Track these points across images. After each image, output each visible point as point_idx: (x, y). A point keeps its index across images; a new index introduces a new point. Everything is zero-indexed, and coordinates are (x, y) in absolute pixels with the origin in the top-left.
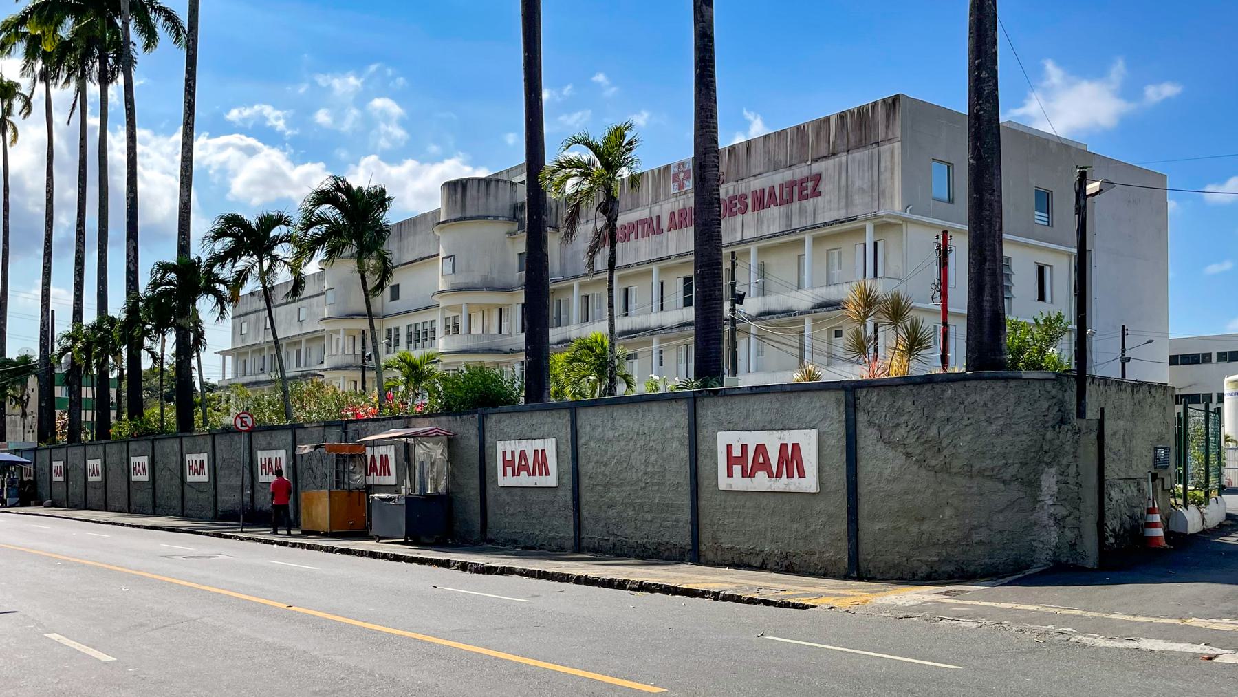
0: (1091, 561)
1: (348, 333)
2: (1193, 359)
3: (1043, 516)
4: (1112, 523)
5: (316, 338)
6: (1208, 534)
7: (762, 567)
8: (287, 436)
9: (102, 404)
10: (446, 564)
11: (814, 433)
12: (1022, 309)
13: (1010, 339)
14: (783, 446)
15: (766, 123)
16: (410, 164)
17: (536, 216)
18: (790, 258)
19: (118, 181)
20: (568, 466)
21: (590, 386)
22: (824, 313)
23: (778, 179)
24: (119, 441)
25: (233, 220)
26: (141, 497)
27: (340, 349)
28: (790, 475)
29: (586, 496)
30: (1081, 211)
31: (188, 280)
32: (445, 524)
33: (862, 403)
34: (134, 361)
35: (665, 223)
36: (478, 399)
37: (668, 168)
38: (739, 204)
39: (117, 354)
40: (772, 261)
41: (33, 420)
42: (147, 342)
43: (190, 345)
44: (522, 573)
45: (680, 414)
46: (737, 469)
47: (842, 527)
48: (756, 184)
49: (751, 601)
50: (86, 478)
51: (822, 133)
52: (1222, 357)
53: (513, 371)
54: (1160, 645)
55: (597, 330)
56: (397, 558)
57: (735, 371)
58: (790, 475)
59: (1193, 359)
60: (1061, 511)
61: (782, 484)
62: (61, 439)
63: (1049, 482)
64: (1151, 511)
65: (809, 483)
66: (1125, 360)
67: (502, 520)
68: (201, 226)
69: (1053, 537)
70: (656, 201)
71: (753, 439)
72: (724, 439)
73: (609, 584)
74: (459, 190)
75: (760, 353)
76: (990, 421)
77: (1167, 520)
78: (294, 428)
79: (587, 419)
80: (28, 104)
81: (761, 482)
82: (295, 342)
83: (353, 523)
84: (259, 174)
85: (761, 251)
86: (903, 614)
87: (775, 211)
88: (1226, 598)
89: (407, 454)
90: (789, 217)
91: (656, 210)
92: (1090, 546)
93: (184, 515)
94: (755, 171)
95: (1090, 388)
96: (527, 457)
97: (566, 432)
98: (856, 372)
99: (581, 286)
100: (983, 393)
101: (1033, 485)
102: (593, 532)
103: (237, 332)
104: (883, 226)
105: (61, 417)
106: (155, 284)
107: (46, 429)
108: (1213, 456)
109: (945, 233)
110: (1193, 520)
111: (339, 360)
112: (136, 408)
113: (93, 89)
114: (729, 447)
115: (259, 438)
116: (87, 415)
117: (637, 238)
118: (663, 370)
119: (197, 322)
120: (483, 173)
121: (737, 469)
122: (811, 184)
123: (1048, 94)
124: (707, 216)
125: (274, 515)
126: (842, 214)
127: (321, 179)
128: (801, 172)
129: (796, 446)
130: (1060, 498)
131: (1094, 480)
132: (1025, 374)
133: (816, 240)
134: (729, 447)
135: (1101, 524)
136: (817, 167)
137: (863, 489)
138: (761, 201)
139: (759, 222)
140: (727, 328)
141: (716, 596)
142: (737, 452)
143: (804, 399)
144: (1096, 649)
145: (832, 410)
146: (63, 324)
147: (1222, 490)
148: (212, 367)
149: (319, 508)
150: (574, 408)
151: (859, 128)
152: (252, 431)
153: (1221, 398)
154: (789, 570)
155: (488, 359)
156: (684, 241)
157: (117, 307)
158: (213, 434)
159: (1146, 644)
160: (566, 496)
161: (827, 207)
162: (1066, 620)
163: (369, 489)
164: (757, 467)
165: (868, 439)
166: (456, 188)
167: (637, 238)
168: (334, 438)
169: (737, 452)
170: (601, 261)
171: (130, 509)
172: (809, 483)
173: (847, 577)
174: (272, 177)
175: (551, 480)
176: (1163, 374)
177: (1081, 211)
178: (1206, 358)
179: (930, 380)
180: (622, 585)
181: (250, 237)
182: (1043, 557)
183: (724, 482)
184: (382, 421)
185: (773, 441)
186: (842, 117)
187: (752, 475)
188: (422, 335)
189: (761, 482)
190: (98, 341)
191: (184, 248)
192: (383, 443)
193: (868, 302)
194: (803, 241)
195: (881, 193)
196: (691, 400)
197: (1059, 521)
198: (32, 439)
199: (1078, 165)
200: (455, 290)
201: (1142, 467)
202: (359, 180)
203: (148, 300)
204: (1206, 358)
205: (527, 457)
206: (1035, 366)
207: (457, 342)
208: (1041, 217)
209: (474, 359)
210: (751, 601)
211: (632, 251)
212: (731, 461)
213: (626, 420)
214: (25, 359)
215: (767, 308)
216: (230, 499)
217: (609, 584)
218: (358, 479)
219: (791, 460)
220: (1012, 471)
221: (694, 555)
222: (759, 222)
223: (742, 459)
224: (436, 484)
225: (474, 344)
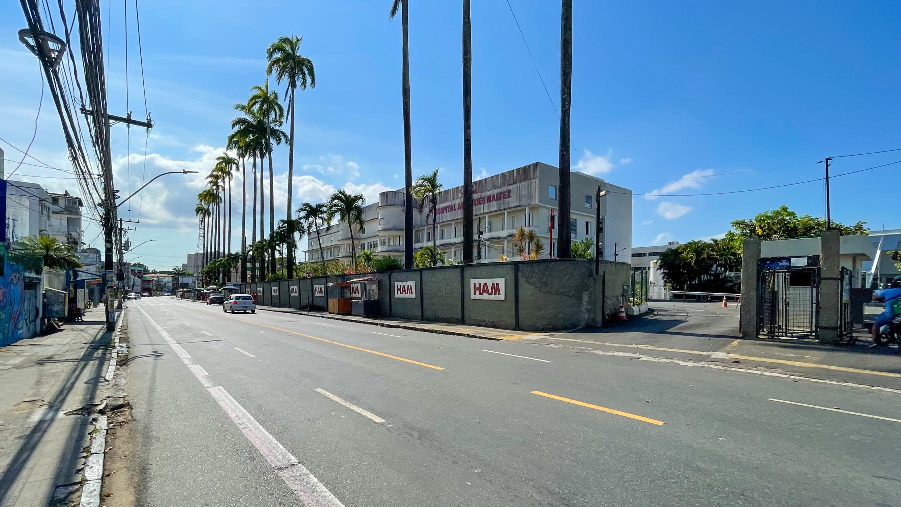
0: (599, 325)
1: (348, 245)
2: (640, 255)
3: (583, 309)
4: (607, 311)
5: (337, 247)
6: (641, 315)
7: (485, 326)
8: (324, 280)
9: (262, 269)
10: (377, 324)
12: (578, 238)
13: (572, 247)
15: (487, 172)
16: (363, 186)
17: (409, 204)
18: (499, 220)
19: (267, 192)
20: (419, 290)
21: (428, 263)
22: (510, 238)
23: (496, 191)
24: (268, 282)
25: (307, 205)
26: (276, 301)
27: (345, 250)
29: (425, 301)
30: (598, 202)
31: (292, 226)
32: (378, 310)
33: (520, 269)
34: (273, 255)
35: (456, 207)
36: (389, 268)
38: (480, 201)
39: (268, 252)
40: (492, 219)
41: (239, 274)
42: (277, 248)
43: (292, 246)
44: (402, 327)
45: (457, 273)
46: (477, 292)
47: (513, 312)
48: (488, 193)
49: (480, 338)
50: (313, 294)
52: (650, 254)
53: (402, 259)
54: (621, 354)
55: (431, 244)
56: (360, 322)
57: (480, 257)
59: (640, 255)
60: (590, 307)
61: (492, 297)
62: (249, 281)
63: (585, 297)
64: (621, 307)
65: (502, 297)
66: (616, 255)
67: (396, 309)
68: (294, 208)
69: (586, 316)
71: (482, 281)
72: (472, 281)
73: (432, 331)
75: (489, 252)
76: (565, 276)
77: (627, 311)
78: (327, 277)
79: (426, 274)
80: (237, 165)
81: (485, 296)
82: (329, 248)
83: (346, 310)
84: (313, 189)
85: (489, 217)
86: (532, 342)
87: (495, 203)
88: (645, 338)
89: (364, 287)
92: (599, 319)
93: (290, 307)
95: (600, 264)
96: (405, 288)
98: (518, 258)
100: (563, 266)
101: (579, 298)
102: (428, 313)
103: (310, 244)
104: (532, 208)
105: (249, 273)
106: (280, 228)
107: (244, 278)
108: (644, 288)
110: (636, 310)
111: (344, 254)
112: (274, 270)
113: (258, 160)
115: (315, 281)
116: (258, 273)
118: (454, 258)
119: (294, 241)
120: (394, 190)
121: (477, 292)
123: (586, 160)
124: (467, 206)
125: (315, 307)
126: (518, 204)
127: (333, 191)
128: (503, 189)
129: (735, 288)
130: (589, 303)
131: (601, 297)
132: (578, 259)
133: (508, 213)
135: (603, 312)
136: (509, 188)
137: (520, 299)
138: (490, 199)
139: (489, 207)
140: (475, 244)
141: (468, 336)
142: (477, 286)
143: (500, 267)
144: (599, 355)
145: (510, 271)
146: (249, 242)
147: (648, 300)
148: (301, 256)
149: (333, 303)
150: (421, 271)
151: (524, 174)
152: (312, 278)
153: (649, 268)
154: (495, 327)
155: (392, 254)
156: (459, 214)
157: (267, 236)
158: (300, 279)
159: (616, 354)
160: (419, 301)
161: (512, 202)
162: (589, 345)
163: (352, 298)
164: (484, 291)
165: (522, 281)
166: (384, 195)
168: (340, 281)
169: (477, 286)
170: (431, 221)
171: (272, 305)
172: (502, 297)
173: (514, 330)
174: (314, 191)
175: (414, 296)
176: (629, 260)
177: (598, 202)
178: (645, 255)
179: (544, 261)
180: (436, 332)
181: (313, 211)
182: (583, 323)
183: (472, 297)
184: (357, 275)
185: (489, 282)
186: (518, 170)
188: (373, 246)
189: (485, 296)
190: (260, 248)
191: (289, 215)
192: (356, 283)
193: (522, 234)
195: (531, 197)
196: (461, 268)
197: (588, 311)
198: (240, 281)
199: (598, 185)
200: (384, 230)
201: (619, 292)
202: (351, 190)
203: (277, 233)
204: (645, 255)
205: (405, 288)
206: (580, 256)
207: (385, 248)
208: (587, 205)
209: (387, 254)
210: (480, 338)
211: (441, 217)
212: (475, 289)
213: (440, 275)
214: (237, 254)
216: (305, 301)
217: (432, 331)
218: (348, 295)
219: (410, 288)
220: (572, 293)
221: (462, 322)
222: (489, 207)
223: (479, 289)
224: (374, 297)
225: (391, 248)
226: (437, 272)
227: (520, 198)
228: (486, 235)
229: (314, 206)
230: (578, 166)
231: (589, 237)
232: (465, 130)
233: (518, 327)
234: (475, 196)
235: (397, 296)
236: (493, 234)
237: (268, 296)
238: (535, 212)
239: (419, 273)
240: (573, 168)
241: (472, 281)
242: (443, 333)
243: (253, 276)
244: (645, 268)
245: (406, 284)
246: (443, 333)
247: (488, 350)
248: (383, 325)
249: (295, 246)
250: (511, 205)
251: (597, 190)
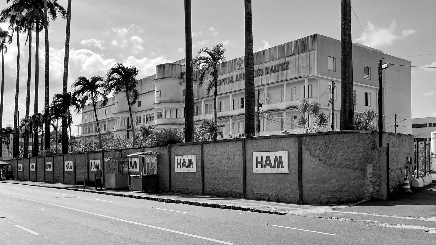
0: (385, 197)
1: (123, 118)
4: (392, 184)
5: (111, 120)
7: (269, 200)
8: (101, 155)
9: (36, 144)
12: (360, 108)
13: (356, 119)
14: (276, 157)
15: (270, 44)
16: (145, 59)
18: (278, 91)
21: (208, 136)
22: (290, 110)
24: (42, 157)
26: (33, 176)
27: (120, 124)
29: (206, 175)
30: (380, 74)
31: (67, 100)
32: (156, 185)
33: (304, 142)
34: (47, 129)
35: (234, 79)
36: (168, 141)
37: (235, 60)
38: (260, 72)
40: (272, 92)
41: (11, 150)
42: (52, 122)
45: (239, 146)
46: (260, 165)
48: (266, 65)
49: (265, 212)
52: (430, 125)
53: (181, 131)
54: (409, 227)
55: (210, 117)
56: (139, 198)
57: (259, 131)
58: (278, 167)
60: (374, 180)
61: (275, 170)
62: (21, 156)
63: (370, 169)
65: (285, 170)
66: (396, 126)
68: (71, 81)
69: (371, 189)
70: (231, 71)
71: (265, 154)
72: (255, 154)
73: (214, 206)
74: (162, 68)
75: (268, 124)
77: (411, 183)
78: (103, 152)
79: (207, 148)
80: (11, 39)
81: (268, 170)
82: (104, 122)
83: (124, 185)
84: (92, 63)
85: (268, 89)
86: (318, 216)
87: (273, 75)
88: (432, 210)
90: (278, 77)
91: (231, 74)
93: (64, 183)
94: (266, 61)
95: (384, 136)
96: (185, 161)
97: (199, 153)
98: (301, 131)
99: (205, 101)
100: (346, 138)
101: (364, 170)
102: (209, 188)
104: (311, 80)
105: (21, 149)
106: (55, 102)
107: (16, 153)
108: (427, 160)
110: (420, 182)
112: (48, 145)
113: (34, 34)
114: (257, 158)
115: (91, 156)
116: (30, 148)
117: (224, 84)
118: (234, 130)
119: (70, 115)
120: (170, 62)
121: (260, 165)
122: (285, 65)
124: (249, 77)
125: (96, 183)
126: (296, 76)
127: (114, 65)
128: (282, 61)
130: (374, 175)
131: (385, 168)
133: (287, 85)
134: (257, 158)
135: (388, 184)
136: (288, 59)
137: (304, 172)
138: (268, 71)
139: (267, 78)
140: (256, 116)
141: (252, 210)
142: (260, 159)
144: (386, 229)
145: (293, 144)
146: (22, 116)
147: (431, 172)
148: (74, 130)
149: (112, 180)
150: (202, 144)
151: (303, 45)
152: (88, 153)
153: (430, 139)
154: (278, 201)
155: (172, 127)
156: (241, 85)
157: (41, 110)
159: (404, 226)
160: (199, 175)
161: (291, 73)
162: (376, 218)
163: (130, 173)
164: (267, 164)
165: (306, 154)
166: (161, 67)
167: (224, 84)
168: (117, 155)
169: (260, 159)
170: (212, 92)
171: (45, 181)
172: (285, 170)
173: (298, 203)
174: (96, 64)
175: (194, 170)
176: (409, 131)
177: (380, 74)
178: (425, 125)
179: (327, 133)
180: (219, 207)
181: (88, 85)
182: (368, 196)
183: (255, 170)
184: (134, 149)
185: (272, 155)
186: (296, 42)
187: (265, 167)
188: (149, 119)
189: (268, 170)
190: (35, 122)
191: (65, 89)
192: (135, 157)
193: (306, 106)
194: (283, 85)
195: (310, 68)
196: (243, 141)
197: (373, 183)
198: (11, 156)
199: (380, 58)
200: (161, 103)
201: (402, 164)
204: (425, 125)
205: (185, 161)
206: (365, 128)
208: (366, 76)
210: (265, 212)
211: (223, 89)
212: (257, 162)
213: (221, 148)
214: (9, 128)
215: (270, 109)
216: (80, 177)
217: (214, 206)
218: (126, 170)
220: (356, 165)
221: (244, 196)
222: (267, 78)
224: (154, 171)
226: (218, 145)
227: (299, 70)
228: (265, 108)
230: (357, 39)
232: (246, 5)
233: (302, 201)
234: (256, 68)
235: (177, 170)
236: (273, 106)
237: (41, 173)
238: (314, 83)
239: (200, 147)
240: (354, 41)
241: (176, 158)
242: (226, 207)
243: (26, 153)
244: (425, 139)
245: (186, 158)
246: (226, 207)
247: (275, 224)
248: (163, 200)
249: (70, 120)
250: (289, 77)
251: (380, 63)
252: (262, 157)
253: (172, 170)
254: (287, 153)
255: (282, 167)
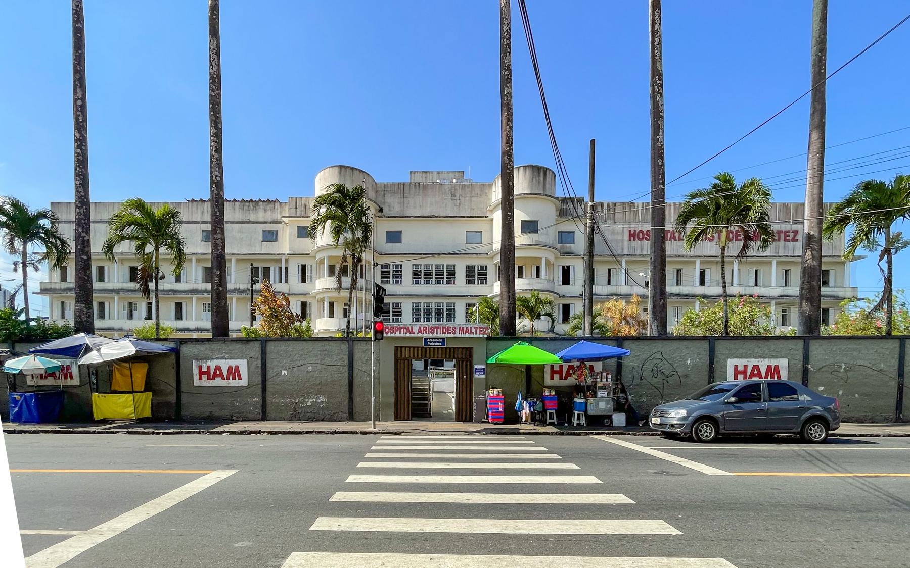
11: (245, 361)
14: (230, 367)
28: (234, 379)
45: (801, 344)
51: (799, 211)
56: (21, 432)
58: (66, 378)
65: (244, 382)
74: (542, 174)
81: (218, 382)
97: (799, 356)
99: (701, 262)
109: (131, 304)
114: (736, 367)
122: (792, 235)
134: (736, 367)
149: (619, 419)
164: (215, 375)
172: (244, 382)
185: (224, 365)
187: (213, 379)
189: (218, 382)
194: (770, 263)
212: (201, 373)
215: (785, 293)
219: (234, 373)
221: (264, 418)
223: (208, 373)
229: (157, 212)
231: (407, 317)
241: (731, 362)
252: (209, 367)
253: (183, 380)
254: (245, 361)
255: (240, 378)
